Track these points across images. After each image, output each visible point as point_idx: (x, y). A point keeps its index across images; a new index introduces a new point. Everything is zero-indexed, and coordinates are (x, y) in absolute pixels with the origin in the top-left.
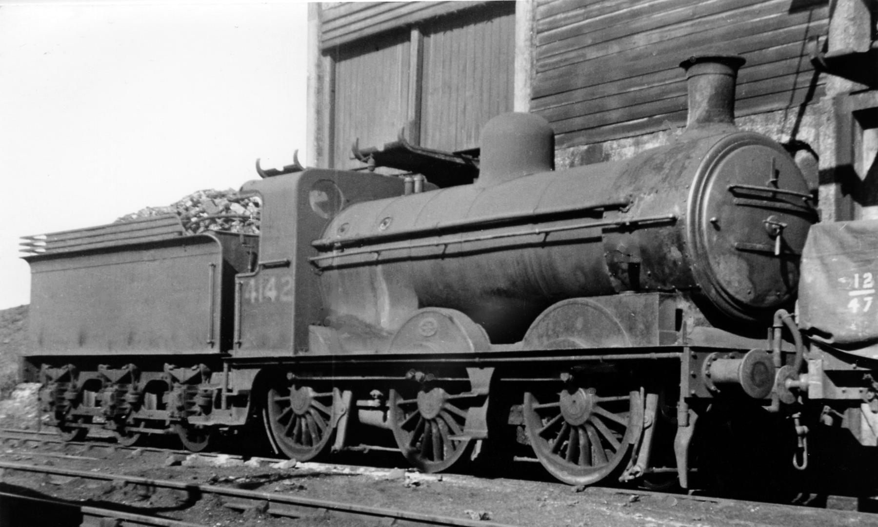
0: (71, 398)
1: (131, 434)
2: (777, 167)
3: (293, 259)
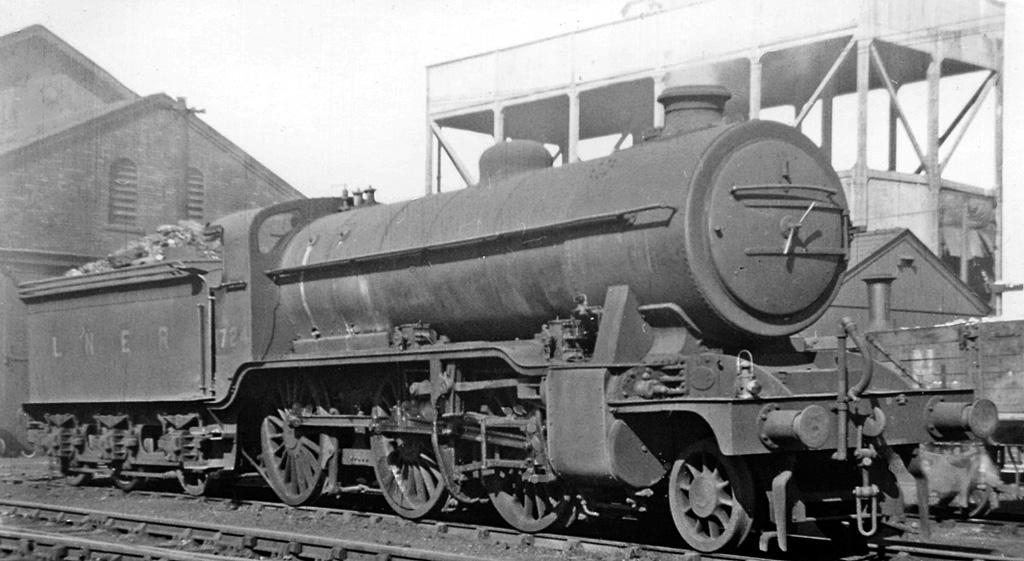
0: (76, 443)
1: (76, 474)
2: (1000, 107)
3: (248, 280)
